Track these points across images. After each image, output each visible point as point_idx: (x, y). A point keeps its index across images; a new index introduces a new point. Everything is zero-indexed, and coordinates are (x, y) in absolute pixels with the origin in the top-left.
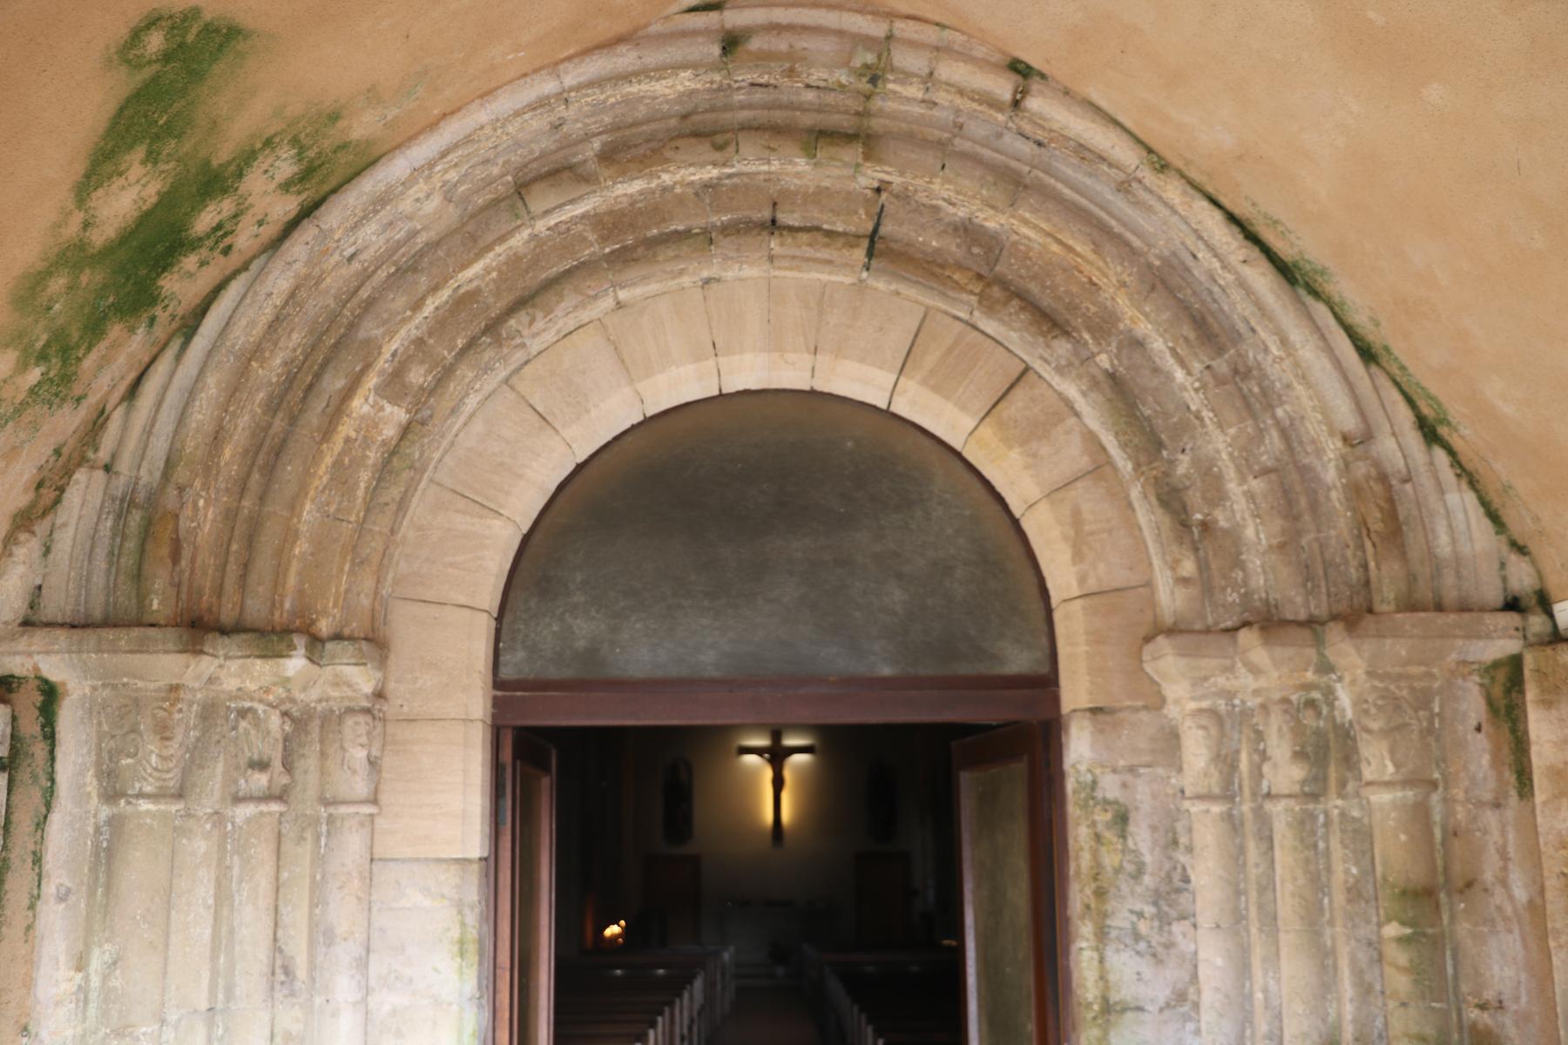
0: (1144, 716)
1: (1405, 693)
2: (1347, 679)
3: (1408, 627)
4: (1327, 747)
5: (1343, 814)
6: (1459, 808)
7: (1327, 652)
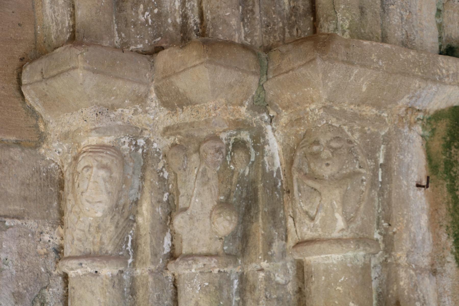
0: (16, 154)
1: (356, 137)
2: (284, 118)
3: (374, 58)
4: (255, 200)
5: (268, 279)
6: (402, 274)
7: (268, 85)
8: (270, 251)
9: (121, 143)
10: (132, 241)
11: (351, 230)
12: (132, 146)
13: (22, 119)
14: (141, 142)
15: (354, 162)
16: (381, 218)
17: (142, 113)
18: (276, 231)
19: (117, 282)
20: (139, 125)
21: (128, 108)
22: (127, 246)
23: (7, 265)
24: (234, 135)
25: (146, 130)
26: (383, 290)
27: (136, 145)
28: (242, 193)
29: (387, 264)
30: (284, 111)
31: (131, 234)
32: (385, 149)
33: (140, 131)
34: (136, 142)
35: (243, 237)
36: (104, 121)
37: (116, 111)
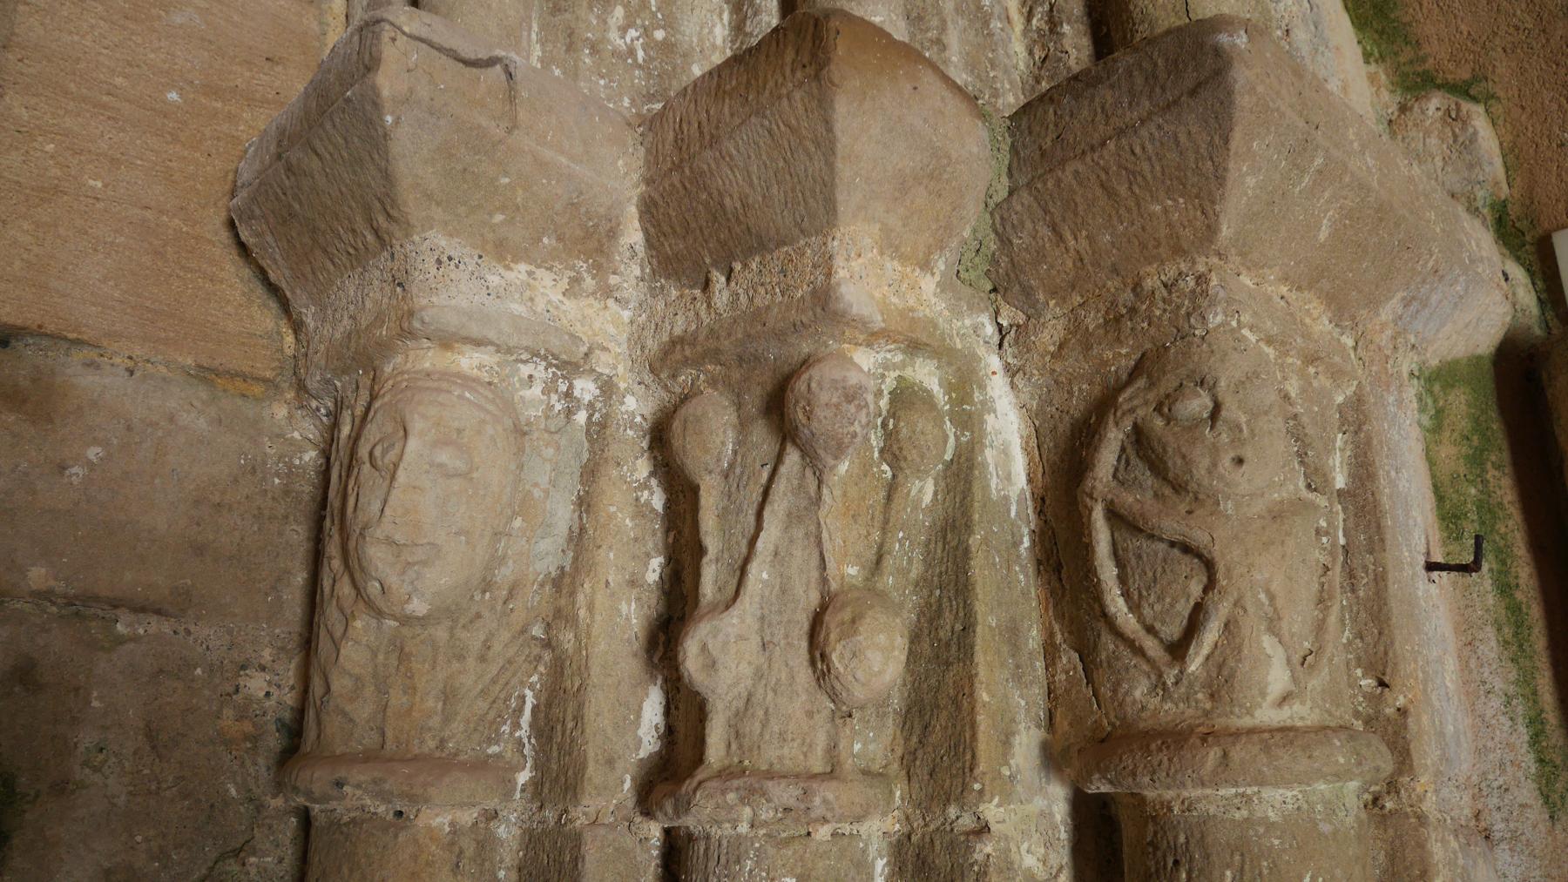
8: (1007, 763)
9: (521, 380)
10: (1096, 595)
12: (554, 397)
13: (229, 309)
14: (585, 388)
17: (594, 293)
18: (1021, 696)
19: (470, 851)
20: (579, 329)
21: (550, 269)
22: (516, 726)
23: (96, 770)
24: (895, 367)
25: (605, 349)
27: (568, 395)
28: (910, 560)
30: (1052, 303)
31: (532, 687)
33: (584, 349)
34: (571, 387)
35: (908, 712)
36: (462, 287)
37: (508, 268)
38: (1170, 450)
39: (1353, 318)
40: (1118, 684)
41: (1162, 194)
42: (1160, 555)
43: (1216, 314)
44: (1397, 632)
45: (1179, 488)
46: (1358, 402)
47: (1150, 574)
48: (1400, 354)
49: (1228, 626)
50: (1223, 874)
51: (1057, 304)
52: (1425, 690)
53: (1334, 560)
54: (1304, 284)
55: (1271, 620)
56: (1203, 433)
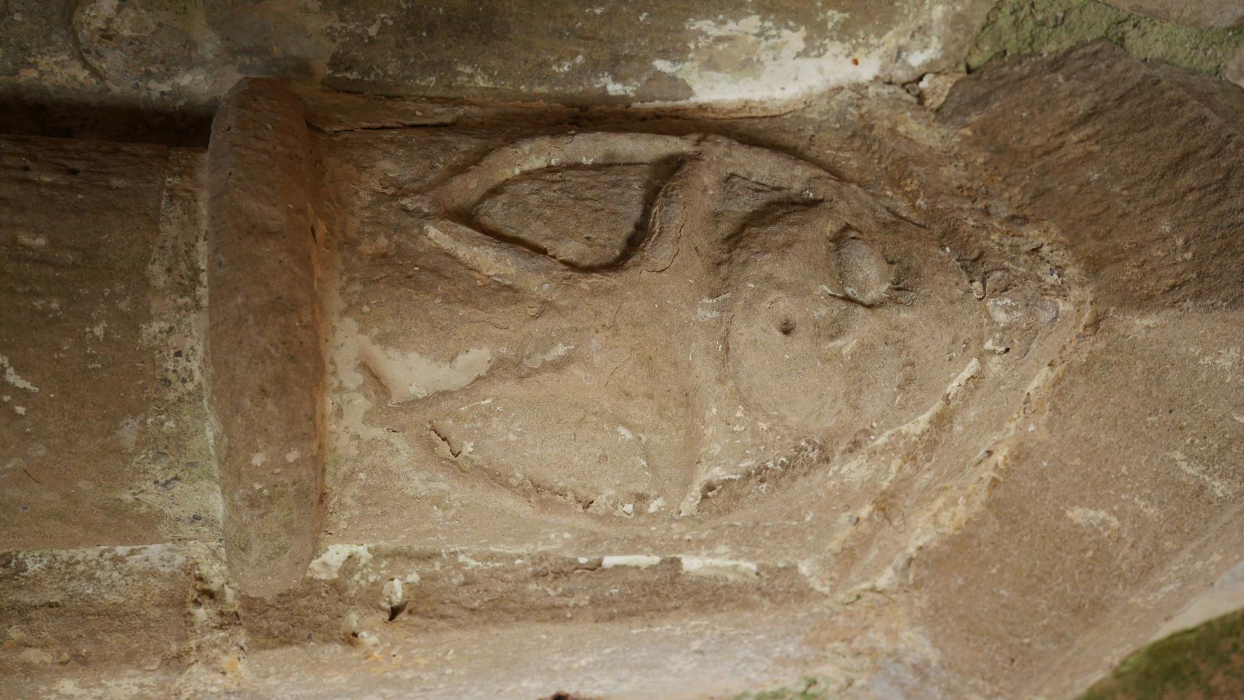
11: (373, 444)
15: (745, 456)
16: (427, 570)
26: (36, 581)
29: (183, 604)
32: (740, 580)
38: (795, 230)
39: (917, 585)
40: (401, 145)
41: (1192, 229)
42: (622, 209)
43: (1008, 310)
44: (475, 634)
45: (735, 240)
46: (802, 594)
47: (589, 194)
48: (850, 661)
49: (508, 293)
50: (38, 232)
51: (965, 137)
52: (384, 682)
53: (599, 518)
54: (999, 493)
55: (517, 365)
56: (824, 281)
